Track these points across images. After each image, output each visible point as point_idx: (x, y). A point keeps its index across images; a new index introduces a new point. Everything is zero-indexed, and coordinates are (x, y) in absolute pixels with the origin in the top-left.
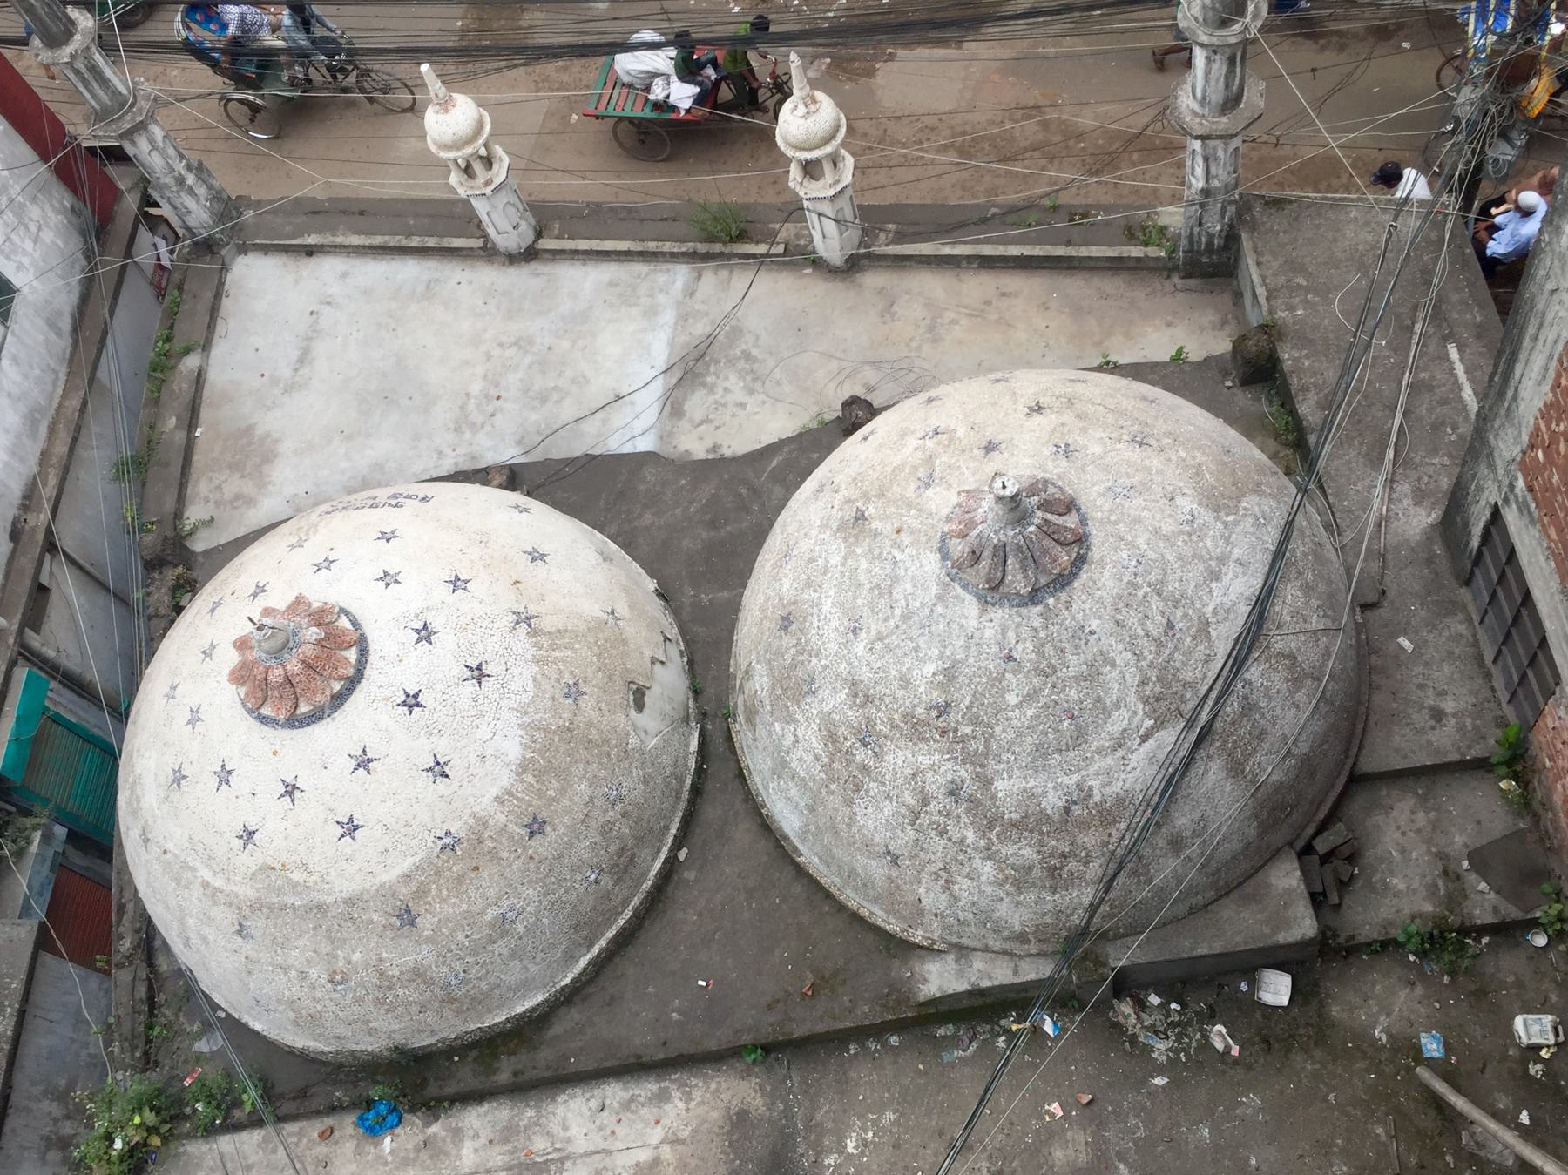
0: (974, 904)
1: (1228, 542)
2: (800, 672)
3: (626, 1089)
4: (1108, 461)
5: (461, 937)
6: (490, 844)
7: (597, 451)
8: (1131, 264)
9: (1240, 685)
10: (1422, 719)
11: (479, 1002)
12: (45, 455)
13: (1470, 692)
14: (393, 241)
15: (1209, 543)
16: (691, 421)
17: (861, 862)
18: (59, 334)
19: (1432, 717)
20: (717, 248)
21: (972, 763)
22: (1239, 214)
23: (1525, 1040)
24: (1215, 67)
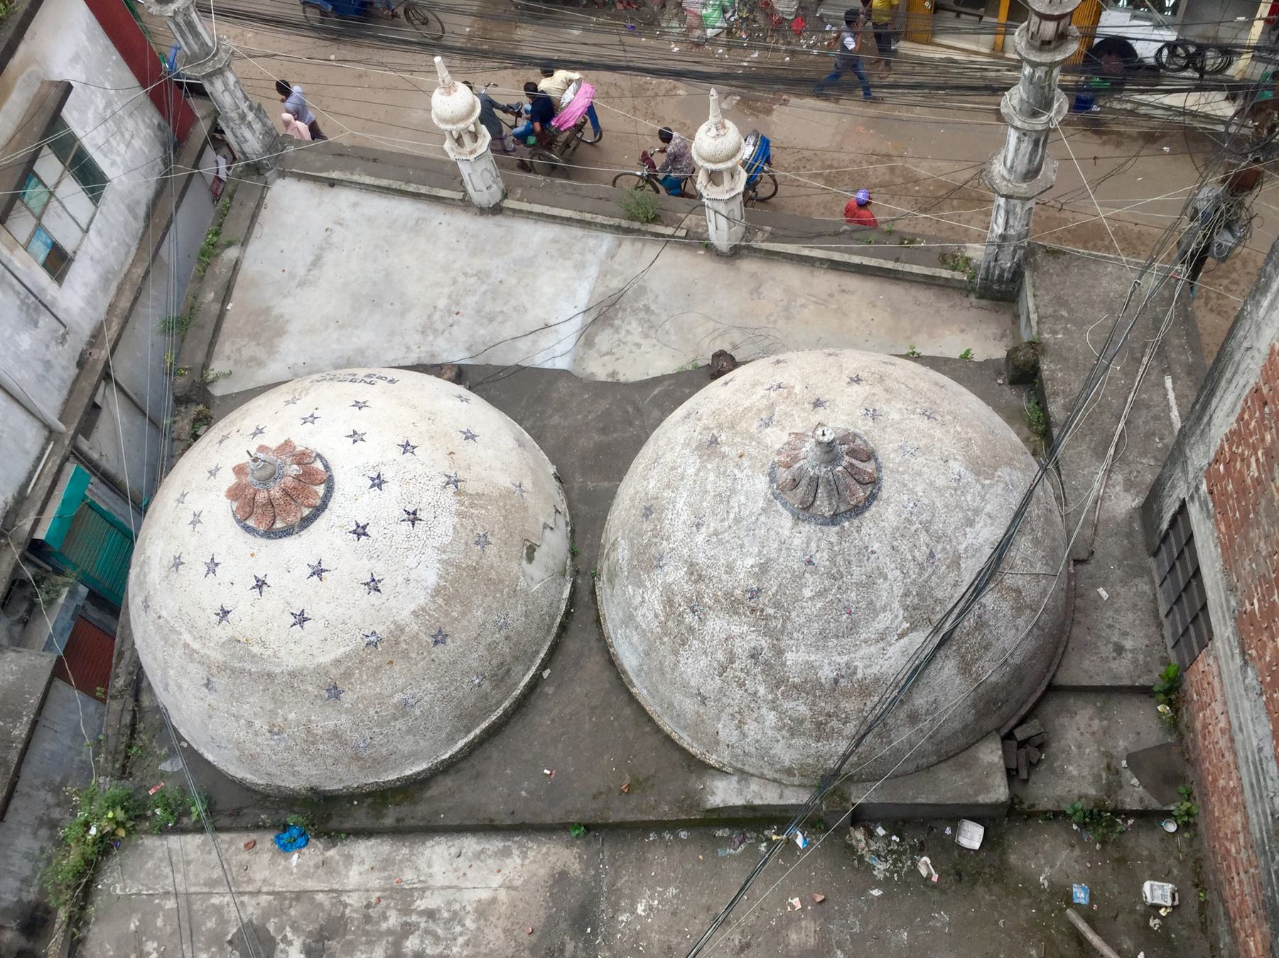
1: (983, 498)
3: (478, 843)
4: (903, 426)
5: (372, 712)
8: (941, 282)
10: (1107, 651)
11: (379, 763)
12: (112, 307)
15: (969, 498)
16: (599, 351)
17: (678, 698)
18: (135, 217)
20: (636, 225)
21: (771, 637)
22: (1026, 257)
23: (1149, 900)
24: (1024, 145)
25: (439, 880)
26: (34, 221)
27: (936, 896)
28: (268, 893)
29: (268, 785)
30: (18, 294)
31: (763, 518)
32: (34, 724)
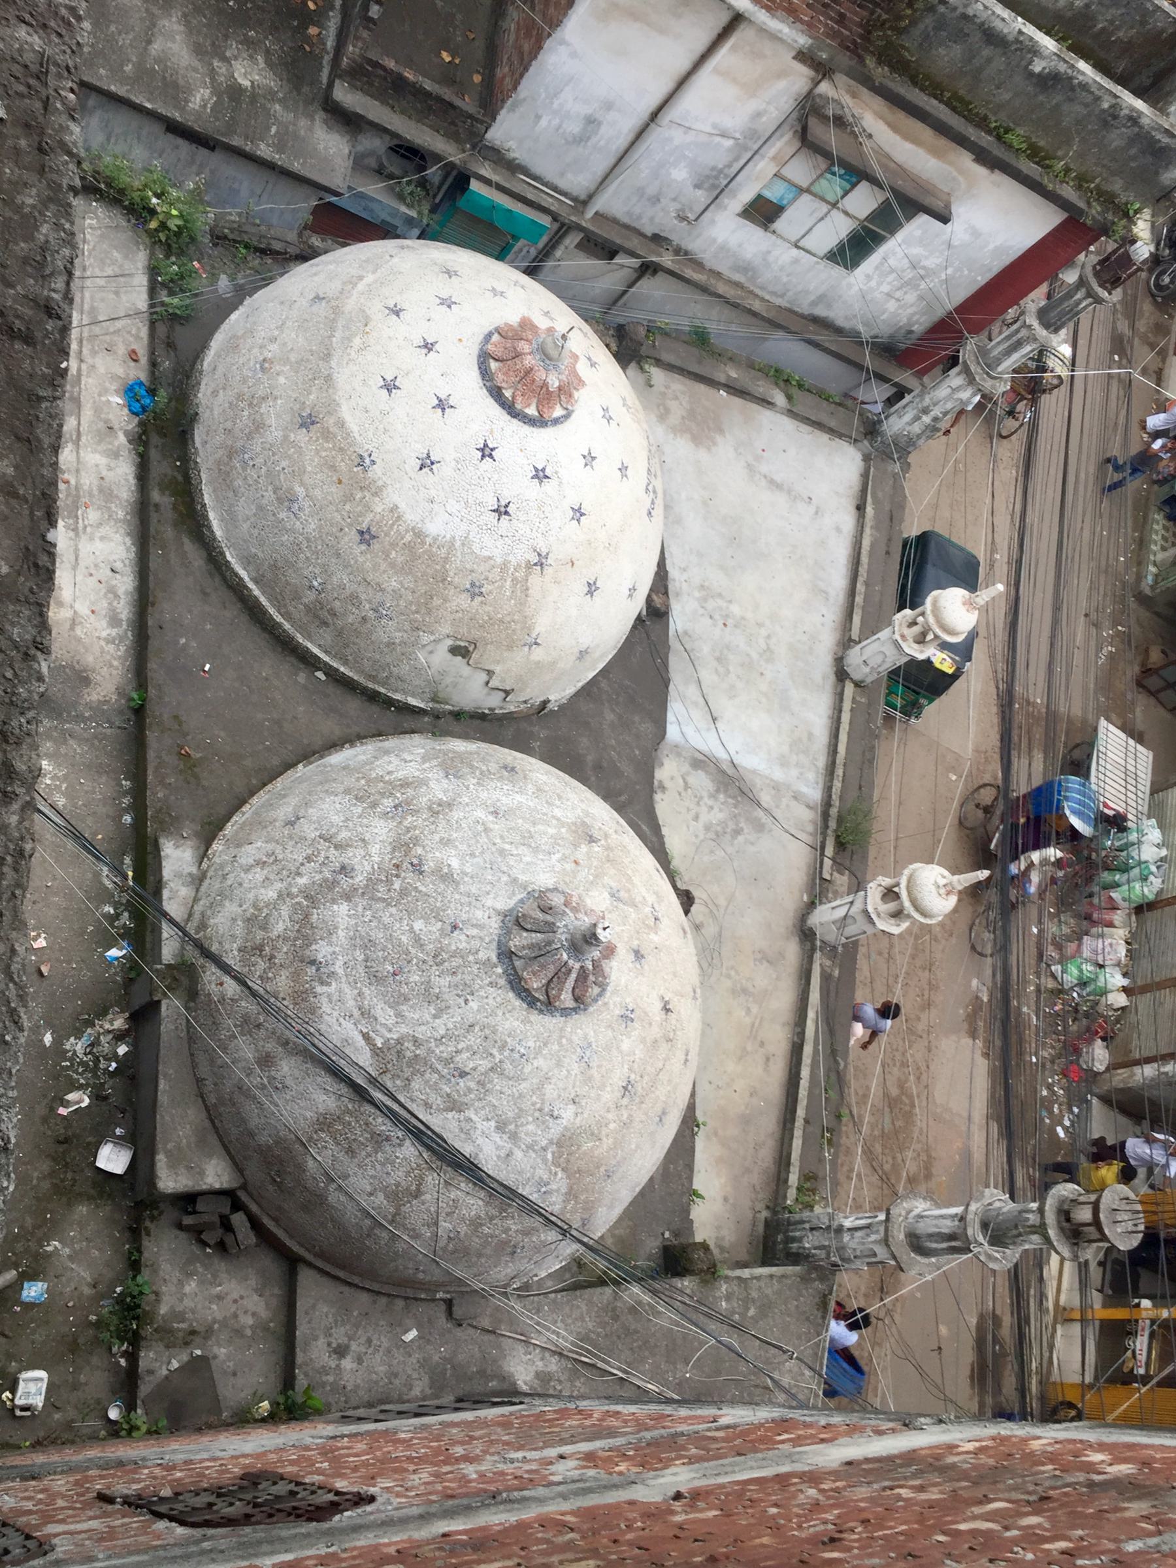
0: (240, 884)
1: (530, 1147)
2: (466, 770)
3: (126, 593)
4: (615, 1052)
5: (284, 464)
6: (359, 496)
7: (671, 687)
8: (783, 1175)
9: (400, 1134)
10: (339, 1335)
11: (224, 476)
12: (718, 275)
13: (357, 1386)
14: (863, 570)
15: (531, 1127)
16: (688, 774)
17: (293, 801)
18: (814, 304)
19: (339, 1346)
20: (833, 824)
21: (367, 886)
22: (817, 1268)
23: (25, 1375)
24: (948, 1223)
25: (85, 547)
26: (805, 185)
27: (41, 1110)
28: (79, 370)
29: (201, 372)
30: (729, 166)
31: (505, 878)
32: (270, 166)
